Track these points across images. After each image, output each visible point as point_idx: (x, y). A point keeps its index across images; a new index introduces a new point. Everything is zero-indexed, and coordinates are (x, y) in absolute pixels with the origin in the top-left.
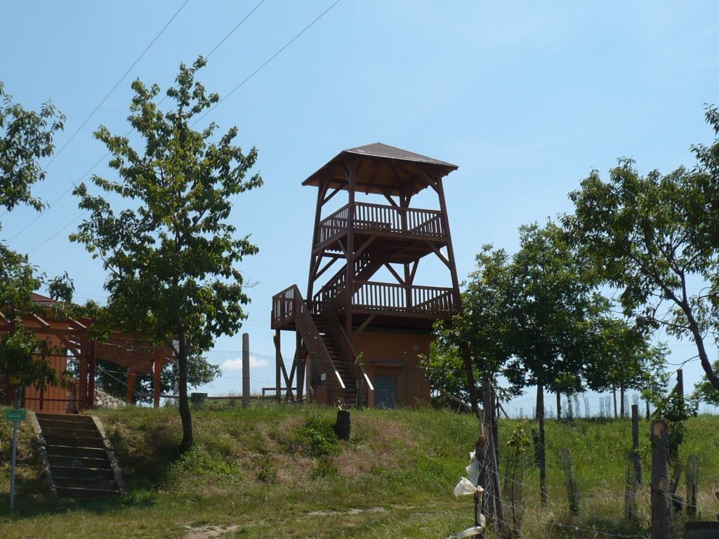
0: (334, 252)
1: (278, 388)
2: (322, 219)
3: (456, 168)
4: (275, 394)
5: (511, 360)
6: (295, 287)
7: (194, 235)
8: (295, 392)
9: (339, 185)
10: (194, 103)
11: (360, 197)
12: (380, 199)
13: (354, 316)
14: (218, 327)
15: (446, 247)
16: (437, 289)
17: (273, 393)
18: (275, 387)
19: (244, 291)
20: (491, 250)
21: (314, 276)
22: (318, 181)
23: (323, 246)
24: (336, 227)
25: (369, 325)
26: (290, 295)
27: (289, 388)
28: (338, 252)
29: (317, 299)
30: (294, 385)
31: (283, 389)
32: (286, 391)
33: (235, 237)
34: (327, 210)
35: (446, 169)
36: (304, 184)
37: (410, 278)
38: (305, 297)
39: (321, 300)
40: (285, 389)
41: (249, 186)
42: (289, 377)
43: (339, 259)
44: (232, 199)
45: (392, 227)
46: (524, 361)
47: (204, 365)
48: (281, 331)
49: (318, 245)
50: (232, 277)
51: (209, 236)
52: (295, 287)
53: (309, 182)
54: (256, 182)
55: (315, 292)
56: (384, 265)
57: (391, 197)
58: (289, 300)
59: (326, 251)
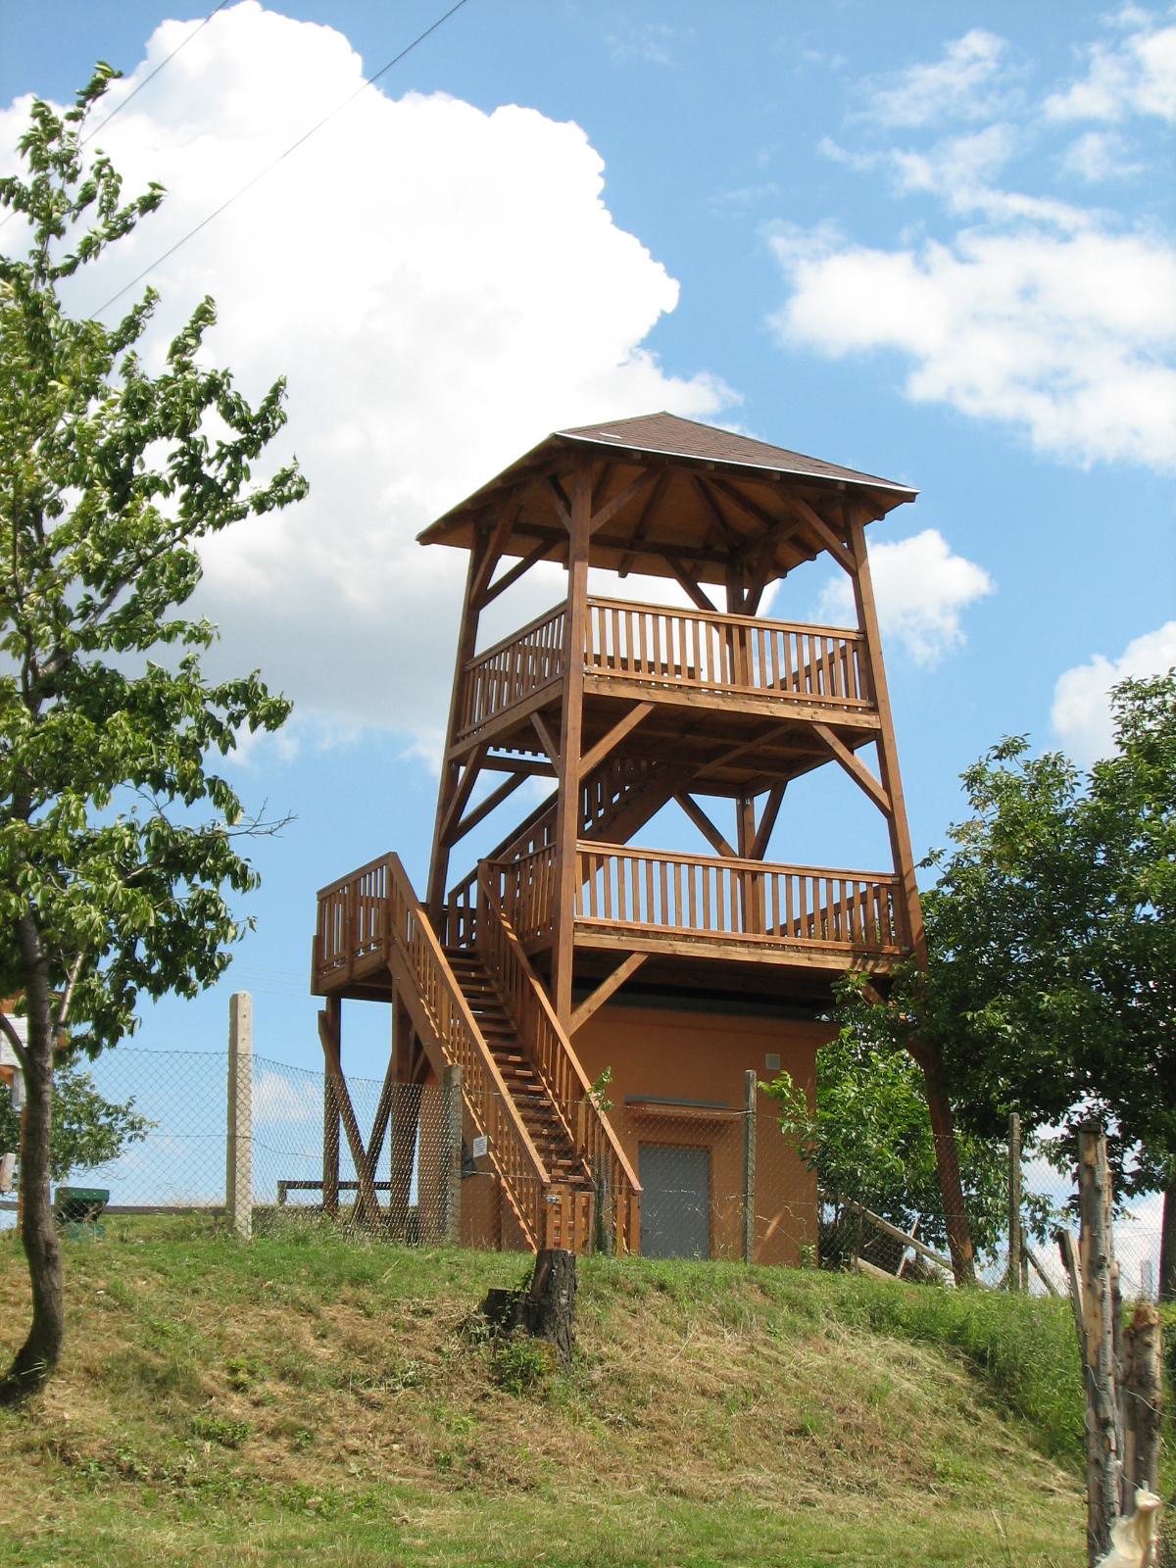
0: (515, 755)
1: (331, 1184)
2: (481, 647)
3: (910, 497)
4: (321, 1201)
5: (1077, 1107)
6: (390, 863)
7: (85, 659)
8: (384, 1198)
9: (534, 543)
10: (91, 221)
11: (602, 581)
12: (668, 591)
13: (581, 954)
14: (155, 969)
15: (874, 743)
16: (828, 876)
17: (316, 1197)
18: (318, 1176)
19: (239, 848)
20: (1022, 757)
21: (451, 829)
22: (468, 531)
23: (484, 735)
24: (523, 678)
25: (626, 987)
26: (376, 887)
27: (368, 1183)
28: (528, 756)
29: (460, 902)
30: (384, 1172)
31: (346, 1185)
32: (354, 1193)
33: (217, 670)
34: (499, 622)
35: (874, 501)
36: (429, 537)
37: (756, 843)
38: (421, 887)
39: (473, 905)
40: (356, 1186)
41: (261, 504)
42: (366, 1142)
43: (532, 778)
44: (212, 547)
45: (704, 677)
46: (1123, 1114)
47: (91, 1108)
48: (348, 1005)
49: (467, 729)
50: (206, 802)
51: (130, 666)
52: (390, 863)
53: (436, 534)
54: (286, 490)
55: (453, 879)
56: (673, 801)
57: (700, 585)
58: (370, 902)
59: (491, 752)
